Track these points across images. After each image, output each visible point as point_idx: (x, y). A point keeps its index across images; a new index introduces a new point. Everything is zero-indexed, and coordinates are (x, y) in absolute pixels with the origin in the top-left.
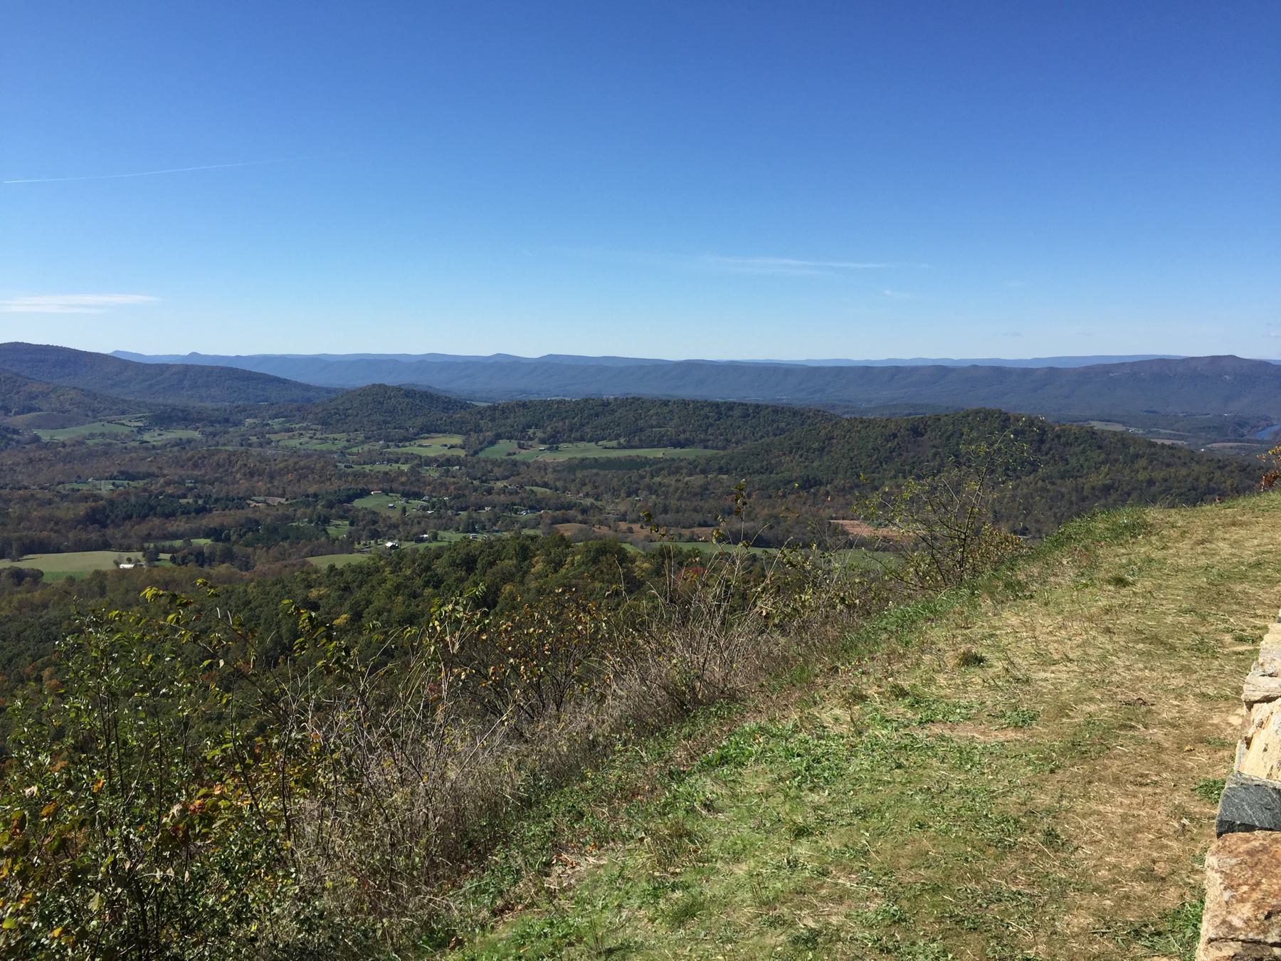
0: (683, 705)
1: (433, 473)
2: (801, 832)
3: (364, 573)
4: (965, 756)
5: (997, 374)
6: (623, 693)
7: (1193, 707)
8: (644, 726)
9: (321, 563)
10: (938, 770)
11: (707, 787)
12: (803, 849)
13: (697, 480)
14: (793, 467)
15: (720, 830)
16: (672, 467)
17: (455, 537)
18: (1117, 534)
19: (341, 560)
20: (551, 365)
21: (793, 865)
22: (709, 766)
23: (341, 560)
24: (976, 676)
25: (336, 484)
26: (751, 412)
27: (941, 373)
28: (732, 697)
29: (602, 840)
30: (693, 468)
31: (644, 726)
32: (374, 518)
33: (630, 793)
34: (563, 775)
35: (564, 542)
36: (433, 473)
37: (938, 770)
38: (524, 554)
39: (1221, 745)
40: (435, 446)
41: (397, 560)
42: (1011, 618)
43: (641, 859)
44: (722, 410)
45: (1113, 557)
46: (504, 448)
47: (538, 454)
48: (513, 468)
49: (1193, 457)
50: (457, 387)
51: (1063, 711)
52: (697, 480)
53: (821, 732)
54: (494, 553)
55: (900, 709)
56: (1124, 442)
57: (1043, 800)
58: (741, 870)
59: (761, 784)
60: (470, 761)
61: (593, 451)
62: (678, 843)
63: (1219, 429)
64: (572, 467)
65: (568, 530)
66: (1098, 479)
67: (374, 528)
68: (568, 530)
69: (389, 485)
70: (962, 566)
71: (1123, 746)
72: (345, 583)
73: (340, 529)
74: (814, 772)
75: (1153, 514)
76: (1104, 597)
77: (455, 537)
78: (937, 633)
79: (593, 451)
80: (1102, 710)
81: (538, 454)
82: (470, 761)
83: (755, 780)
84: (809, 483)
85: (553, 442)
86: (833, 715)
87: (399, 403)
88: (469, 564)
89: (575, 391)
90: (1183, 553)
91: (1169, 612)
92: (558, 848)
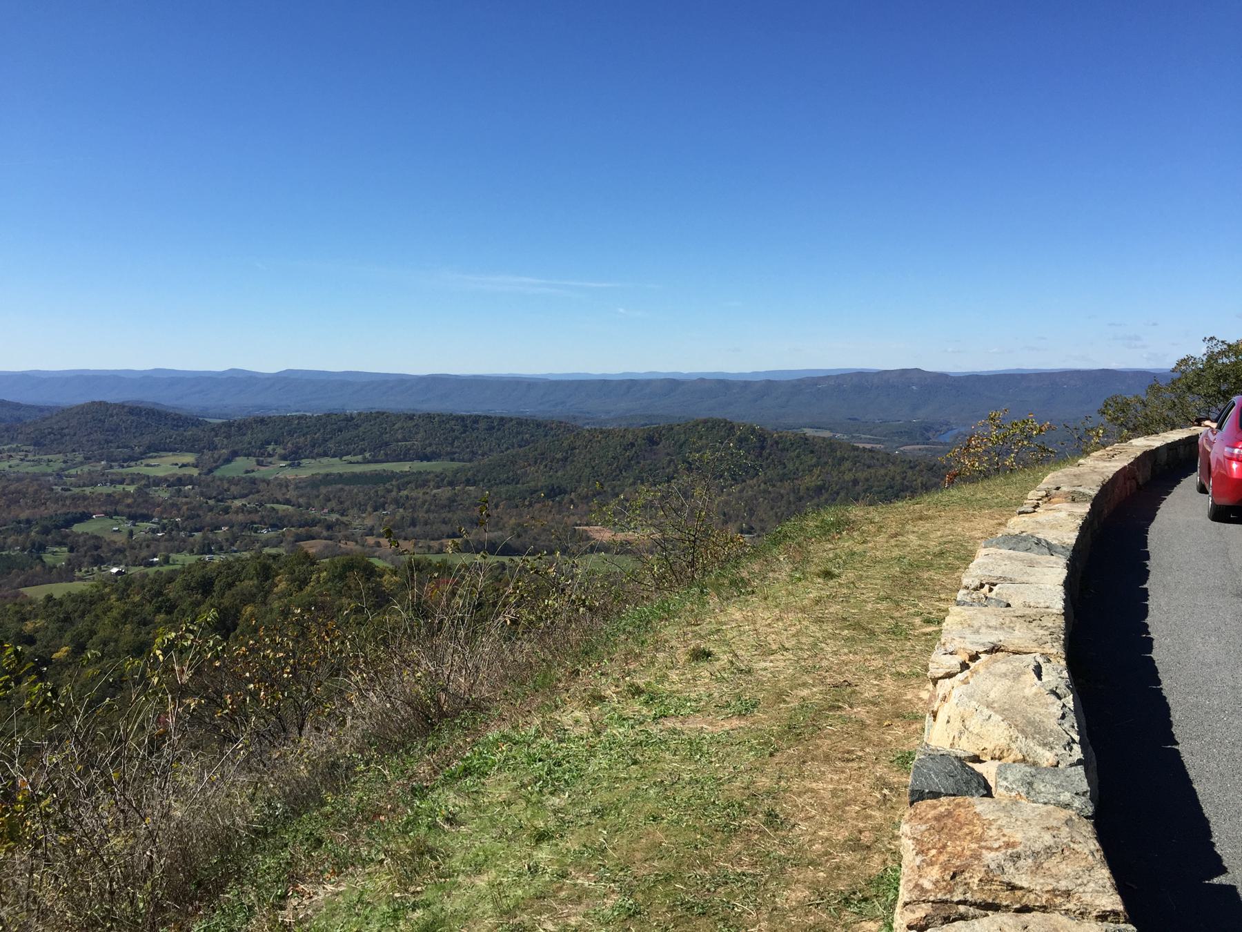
0: (429, 718)
1: (163, 494)
2: (541, 837)
3: (87, 603)
4: (694, 747)
5: (722, 387)
6: (366, 704)
7: (889, 684)
8: (389, 742)
9: (36, 593)
10: (670, 762)
11: (451, 800)
12: (543, 854)
13: (445, 493)
14: (538, 477)
15: (461, 844)
16: (420, 480)
17: (185, 559)
18: (826, 531)
19: (59, 590)
20: (288, 381)
21: (534, 870)
22: (454, 777)
23: (59, 590)
24: (704, 670)
25: (52, 509)
26: (495, 425)
27: (673, 385)
28: (477, 707)
29: (341, 866)
30: (441, 480)
31: (389, 742)
32: (96, 543)
33: (371, 815)
34: (301, 801)
35: (310, 560)
36: (163, 494)
37: (670, 762)
38: (266, 573)
39: (913, 718)
40: (164, 466)
41: (124, 585)
42: (736, 613)
43: (378, 882)
44: (467, 423)
45: (822, 552)
46: (241, 465)
47: (278, 470)
48: (251, 485)
49: (889, 459)
50: (190, 403)
51: (780, 696)
52: (445, 493)
53: (562, 735)
54: (233, 574)
55: (636, 707)
56: (831, 445)
57: (764, 782)
58: (482, 882)
59: (503, 793)
60: (203, 793)
61: (337, 466)
62: (420, 861)
63: (909, 434)
64: (315, 483)
65: (312, 547)
66: (810, 481)
67: (98, 553)
68: (312, 547)
69: (112, 507)
70: (694, 567)
71: (832, 726)
72: (63, 615)
73: (58, 556)
74: (556, 774)
75: (856, 512)
76: (815, 589)
77: (185, 559)
78: (669, 631)
79: (337, 466)
80: (813, 693)
81: (278, 470)
82: (203, 793)
83: (497, 789)
84: (554, 492)
85: (294, 458)
86: (574, 717)
87: (123, 422)
88: (206, 586)
89: (317, 406)
90: (880, 546)
91: (869, 600)
92: (294, 879)
